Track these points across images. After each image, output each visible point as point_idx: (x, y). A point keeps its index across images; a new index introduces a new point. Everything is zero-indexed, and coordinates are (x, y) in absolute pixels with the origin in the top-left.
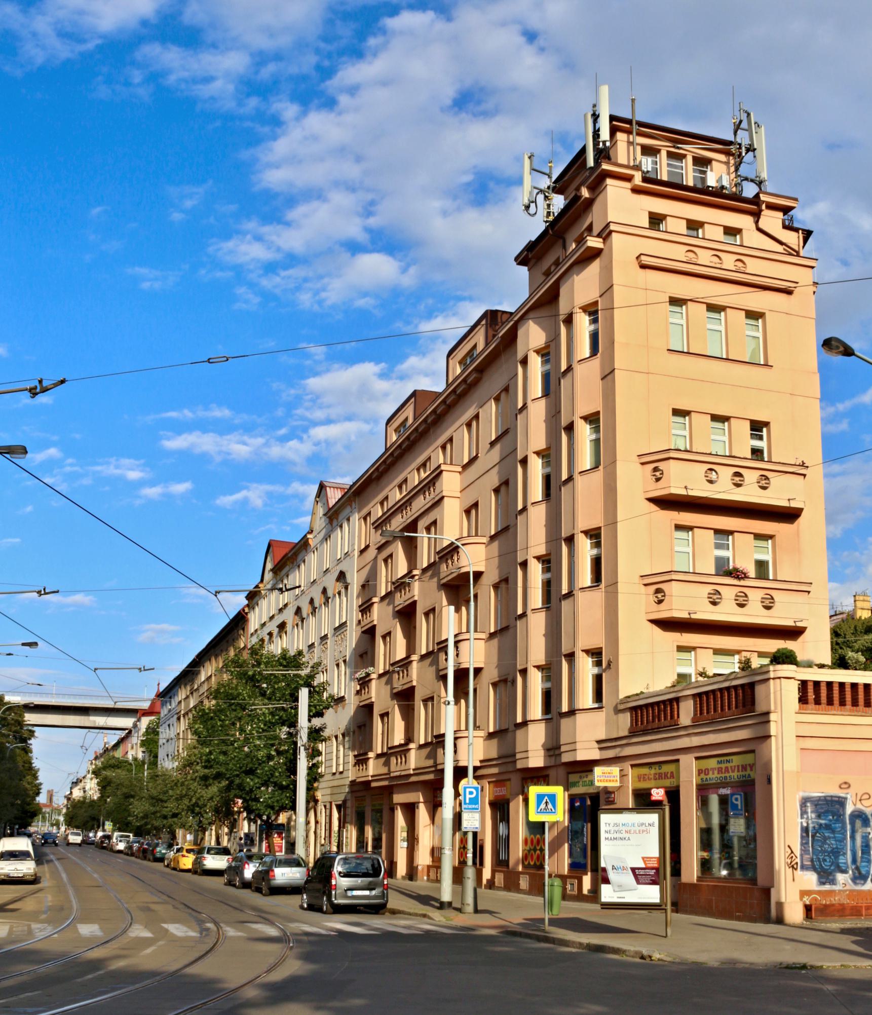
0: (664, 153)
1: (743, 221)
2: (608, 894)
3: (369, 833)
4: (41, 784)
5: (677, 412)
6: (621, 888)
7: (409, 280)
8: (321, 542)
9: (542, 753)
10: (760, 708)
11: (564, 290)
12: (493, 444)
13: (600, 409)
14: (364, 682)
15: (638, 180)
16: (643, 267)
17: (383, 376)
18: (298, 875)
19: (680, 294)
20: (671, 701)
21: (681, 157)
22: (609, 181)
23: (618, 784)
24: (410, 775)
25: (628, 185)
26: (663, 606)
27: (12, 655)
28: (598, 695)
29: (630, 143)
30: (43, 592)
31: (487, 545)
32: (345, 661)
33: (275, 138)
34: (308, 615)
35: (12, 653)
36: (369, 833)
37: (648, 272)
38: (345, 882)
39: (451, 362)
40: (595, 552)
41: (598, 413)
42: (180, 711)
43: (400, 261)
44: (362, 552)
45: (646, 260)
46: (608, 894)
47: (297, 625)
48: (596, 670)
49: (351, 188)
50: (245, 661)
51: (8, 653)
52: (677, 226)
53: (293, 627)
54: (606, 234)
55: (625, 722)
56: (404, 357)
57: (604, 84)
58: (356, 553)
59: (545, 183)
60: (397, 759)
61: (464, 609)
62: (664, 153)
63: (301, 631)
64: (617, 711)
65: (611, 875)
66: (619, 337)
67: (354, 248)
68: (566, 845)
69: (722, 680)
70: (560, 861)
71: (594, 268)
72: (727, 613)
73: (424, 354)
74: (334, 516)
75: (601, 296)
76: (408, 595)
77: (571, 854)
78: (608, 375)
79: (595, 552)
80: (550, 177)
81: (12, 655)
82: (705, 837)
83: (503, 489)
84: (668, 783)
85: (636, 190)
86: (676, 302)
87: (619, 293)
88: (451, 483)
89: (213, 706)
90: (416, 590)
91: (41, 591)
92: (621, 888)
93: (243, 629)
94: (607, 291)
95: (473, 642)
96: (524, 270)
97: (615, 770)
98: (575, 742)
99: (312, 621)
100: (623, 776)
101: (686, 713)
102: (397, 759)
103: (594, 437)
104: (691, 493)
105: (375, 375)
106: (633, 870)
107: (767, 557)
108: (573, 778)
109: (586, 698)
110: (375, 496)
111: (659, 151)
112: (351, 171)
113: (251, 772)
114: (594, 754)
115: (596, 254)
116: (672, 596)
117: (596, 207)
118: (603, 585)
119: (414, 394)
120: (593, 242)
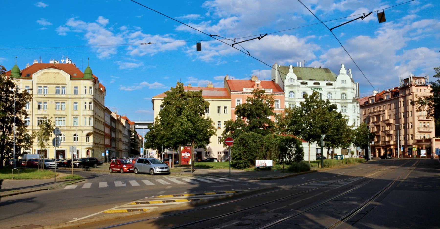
1: (426, 88)
4: (304, 152)
10: (432, 141)
14: (167, 141)
27: (151, 43)
28: (412, 138)
30: (261, 37)
35: (150, 42)
42: (414, 170)
50: (419, 99)
51: (148, 43)
55: (416, 141)
60: (219, 90)
72: (425, 131)
81: (151, 43)
89: (24, 142)
91: (260, 37)
101: (423, 141)
102: (219, 90)
107: (429, 125)
109: (411, 139)
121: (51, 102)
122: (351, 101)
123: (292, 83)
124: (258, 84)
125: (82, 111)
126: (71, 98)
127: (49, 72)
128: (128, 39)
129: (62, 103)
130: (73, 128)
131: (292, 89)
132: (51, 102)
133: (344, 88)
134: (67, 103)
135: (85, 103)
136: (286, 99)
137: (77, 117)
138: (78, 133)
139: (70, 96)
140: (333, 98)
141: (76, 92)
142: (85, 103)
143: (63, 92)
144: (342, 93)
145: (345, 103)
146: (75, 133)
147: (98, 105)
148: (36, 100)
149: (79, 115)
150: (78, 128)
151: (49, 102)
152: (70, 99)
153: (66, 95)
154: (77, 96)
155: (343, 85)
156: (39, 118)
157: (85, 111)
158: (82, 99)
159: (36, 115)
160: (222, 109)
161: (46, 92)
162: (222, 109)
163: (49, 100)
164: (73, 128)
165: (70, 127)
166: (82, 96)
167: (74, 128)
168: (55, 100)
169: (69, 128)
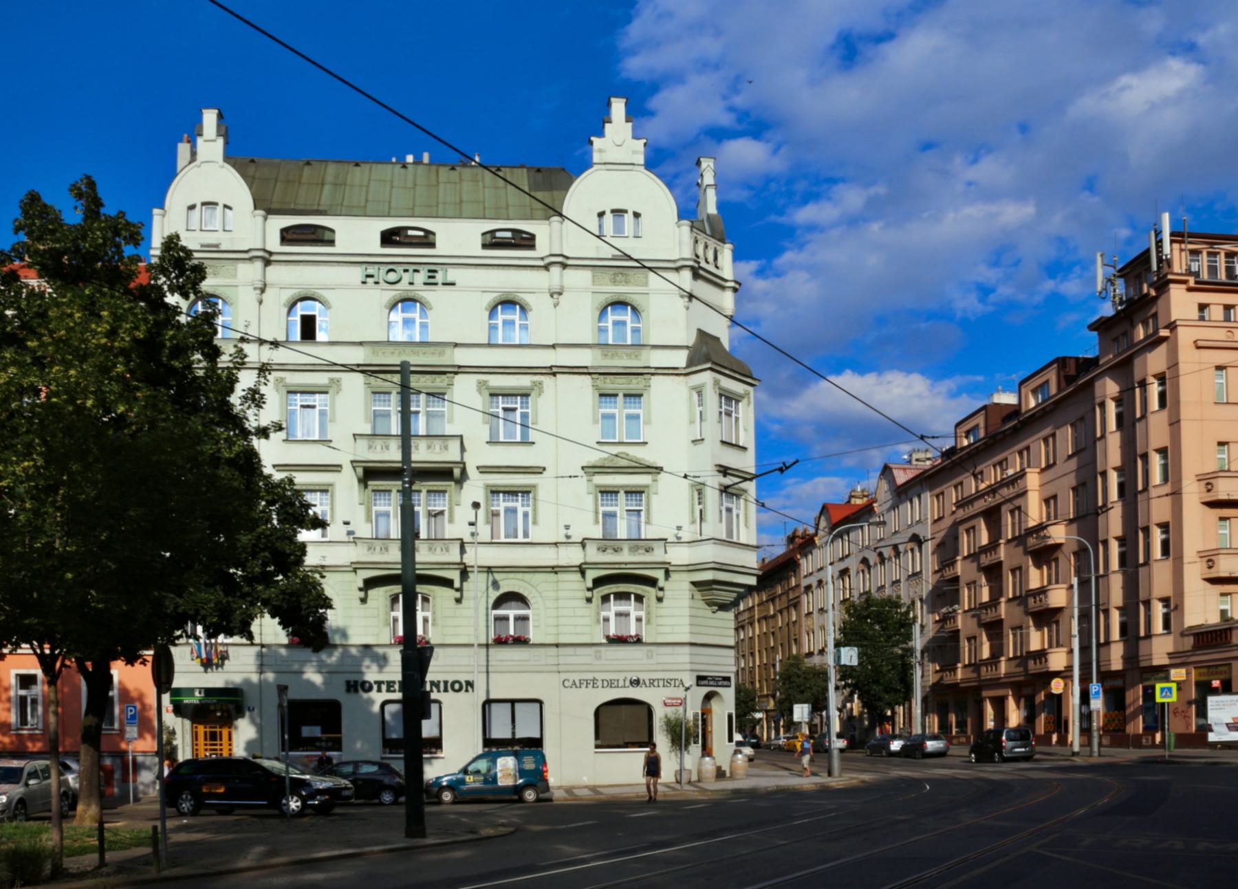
0: (1205, 254)
2: (1212, 737)
3: (953, 718)
5: (1221, 444)
6: (1220, 734)
7: (778, 165)
8: (889, 510)
9: (1121, 661)
11: (1137, 362)
12: (1070, 457)
13: (1168, 444)
15: (1192, 283)
16: (1198, 348)
17: (760, 273)
18: (942, 745)
19: (1220, 362)
20: (1226, 630)
21: (1215, 254)
22: (1172, 286)
23: (1184, 678)
24: (1001, 678)
25: (1184, 286)
26: (1213, 570)
28: (1167, 624)
29: (1181, 250)
31: (1066, 525)
32: (921, 600)
33: (629, 20)
34: (876, 564)
36: (953, 718)
37: (1202, 350)
38: (1010, 744)
39: (1023, 390)
40: (1164, 536)
41: (1166, 448)
43: (768, 141)
44: (935, 521)
45: (1200, 343)
46: (1212, 737)
47: (863, 571)
48: (1165, 610)
49: (705, 66)
52: (1216, 313)
53: (858, 572)
54: (1172, 326)
55: (1189, 642)
56: (780, 251)
57: (1165, 212)
58: (929, 522)
59: (1111, 271)
61: (1045, 568)
62: (1205, 254)
63: (868, 576)
64: (1183, 635)
65: (1214, 728)
66: (1184, 397)
67: (718, 135)
68: (1141, 717)
69: (457, 351)
70: (1137, 726)
71: (1162, 350)
73: (801, 247)
74: (903, 493)
75: (1168, 368)
76: (994, 556)
77: (1144, 721)
78: (1175, 423)
79: (1164, 536)
80: (1115, 267)
82: (1085, 725)
83: (1080, 489)
84: (1223, 677)
85: (1190, 290)
86: (1220, 368)
87: (1183, 368)
88: (1033, 480)
90: (1002, 553)
92: (1220, 734)
93: (795, 572)
94: (1174, 365)
95: (303, 417)
96: (1095, 333)
97: (1183, 671)
98: (691, 616)
99: (878, 571)
100: (1188, 673)
103: (1162, 462)
104: (1231, 498)
105: (751, 274)
106: (1227, 724)
108: (1145, 676)
109: (1158, 627)
110: (951, 479)
111: (1201, 252)
112: (709, 46)
113: (876, 682)
114: (1166, 661)
115: (1165, 339)
116: (731, 318)
117: (1160, 302)
118: (1171, 558)
119: (985, 408)
120: (1164, 333)
122: (679, 359)
144: (602, 299)
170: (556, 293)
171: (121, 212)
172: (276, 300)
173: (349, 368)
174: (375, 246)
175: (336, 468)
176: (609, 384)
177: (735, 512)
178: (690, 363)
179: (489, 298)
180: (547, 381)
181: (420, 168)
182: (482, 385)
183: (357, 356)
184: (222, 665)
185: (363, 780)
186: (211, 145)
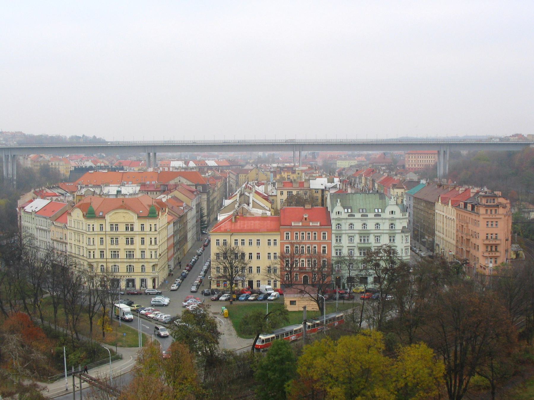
19: (492, 221)
121: (122, 238)
122: (400, 231)
123: (339, 216)
124: (306, 219)
125: (148, 246)
126: (139, 234)
127: (118, 212)
128: (400, 351)
129: (116, 238)
130: (141, 260)
131: (339, 221)
132: (122, 238)
133: (393, 219)
134: (135, 238)
135: (151, 239)
136: (333, 232)
137: (144, 250)
138: (145, 265)
139: (137, 233)
140: (380, 229)
141: (142, 228)
142: (151, 239)
143: (132, 229)
144: (390, 223)
145: (393, 233)
146: (143, 264)
147: (84, 234)
148: (109, 236)
149: (146, 249)
150: (146, 260)
151: (120, 238)
152: (138, 235)
153: (135, 231)
154: (143, 233)
155: (391, 216)
156: (127, 252)
157: (151, 246)
158: (148, 235)
159: (109, 249)
160: (272, 242)
161: (117, 229)
162: (272, 242)
163: (119, 236)
164: (141, 260)
165: (138, 259)
166: (148, 233)
167: (142, 260)
168: (125, 236)
169: (137, 260)
170: (384, 223)
171: (403, 227)
172: (348, 224)
173: (356, 233)
174: (360, 217)
175: (355, 246)
176: (361, 235)
177: (464, 227)
178: (401, 232)
179: (375, 223)
180: (382, 234)
181: (362, 208)
182: (374, 235)
183: (357, 232)
184: (6, 397)
185: (342, 299)
186: (339, 204)
